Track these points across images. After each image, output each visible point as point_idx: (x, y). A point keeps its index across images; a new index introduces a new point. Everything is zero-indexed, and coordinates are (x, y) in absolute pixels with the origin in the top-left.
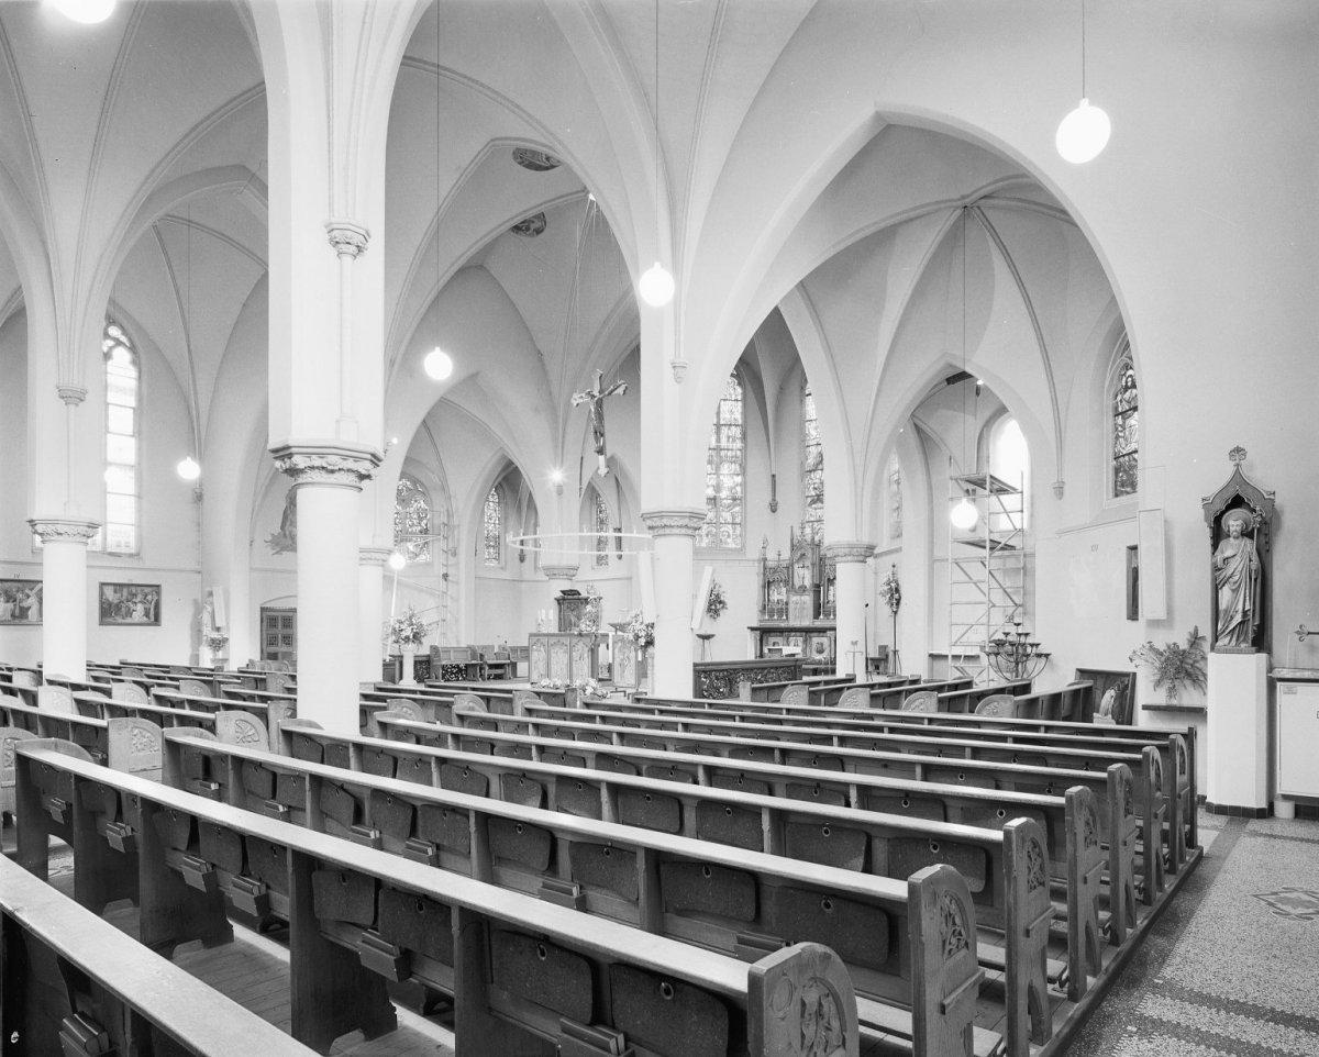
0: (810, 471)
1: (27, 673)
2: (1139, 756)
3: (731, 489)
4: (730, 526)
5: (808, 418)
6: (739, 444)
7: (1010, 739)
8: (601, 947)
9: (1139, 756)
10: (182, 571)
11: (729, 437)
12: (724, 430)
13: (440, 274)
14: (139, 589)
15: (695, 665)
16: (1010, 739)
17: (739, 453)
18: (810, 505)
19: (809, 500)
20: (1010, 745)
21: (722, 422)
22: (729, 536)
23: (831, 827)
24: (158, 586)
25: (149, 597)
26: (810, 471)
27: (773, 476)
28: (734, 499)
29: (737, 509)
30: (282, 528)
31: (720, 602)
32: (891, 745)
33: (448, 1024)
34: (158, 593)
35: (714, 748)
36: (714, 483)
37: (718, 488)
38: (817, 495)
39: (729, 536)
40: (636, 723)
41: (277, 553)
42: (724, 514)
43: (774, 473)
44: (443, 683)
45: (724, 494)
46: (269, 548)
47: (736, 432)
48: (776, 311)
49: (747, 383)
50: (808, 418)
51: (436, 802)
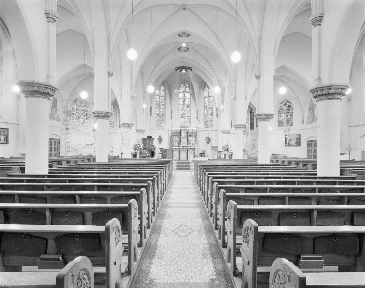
2: (147, 184)
5: (179, 98)
8: (110, 253)
9: (147, 184)
10: (310, 128)
12: (161, 98)
13: (152, 47)
14: (3, 130)
16: (318, 178)
19: (180, 117)
20: (282, 180)
23: (33, 211)
24: (7, 129)
25: (5, 133)
27: (197, 111)
30: (51, 111)
32: (139, 182)
34: (8, 132)
35: (271, 183)
44: (12, 167)
45: (161, 113)
49: (166, 86)
50: (179, 98)
51: (142, 206)
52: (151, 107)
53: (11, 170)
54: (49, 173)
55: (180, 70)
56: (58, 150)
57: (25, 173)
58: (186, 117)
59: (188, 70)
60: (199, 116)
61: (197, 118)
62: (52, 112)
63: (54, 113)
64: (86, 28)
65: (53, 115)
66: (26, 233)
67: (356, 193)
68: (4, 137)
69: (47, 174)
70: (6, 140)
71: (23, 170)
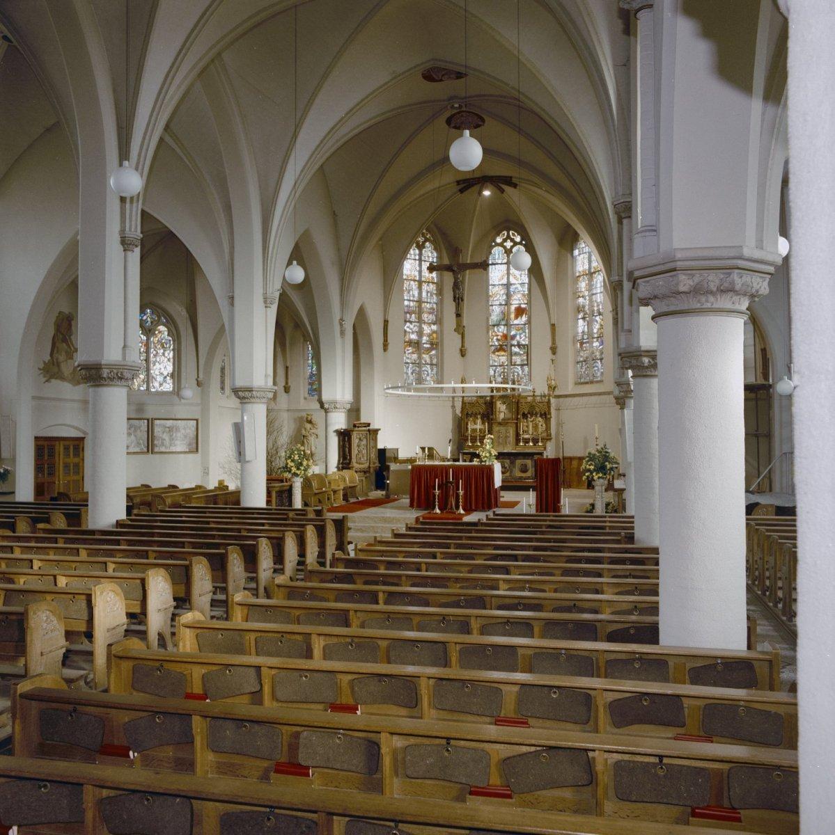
0: (494, 326)
1: (99, 565)
3: (429, 335)
4: (428, 366)
6: (435, 299)
7: (473, 531)
11: (428, 292)
12: (425, 287)
15: (37, 438)
16: (473, 531)
17: (435, 306)
18: (494, 352)
19: (493, 348)
21: (423, 279)
22: (428, 375)
26: (494, 326)
28: (432, 344)
29: (433, 352)
30: (51, 355)
31: (310, 422)
33: (18, 833)
36: (417, 330)
37: (420, 333)
38: (500, 345)
39: (428, 375)
40: (394, 554)
41: (47, 381)
42: (424, 356)
43: (553, 322)
45: (425, 339)
46: (42, 376)
47: (432, 287)
48: (143, 212)
52: (386, 322)
58: (516, 349)
59: (504, 187)
62: (55, 355)
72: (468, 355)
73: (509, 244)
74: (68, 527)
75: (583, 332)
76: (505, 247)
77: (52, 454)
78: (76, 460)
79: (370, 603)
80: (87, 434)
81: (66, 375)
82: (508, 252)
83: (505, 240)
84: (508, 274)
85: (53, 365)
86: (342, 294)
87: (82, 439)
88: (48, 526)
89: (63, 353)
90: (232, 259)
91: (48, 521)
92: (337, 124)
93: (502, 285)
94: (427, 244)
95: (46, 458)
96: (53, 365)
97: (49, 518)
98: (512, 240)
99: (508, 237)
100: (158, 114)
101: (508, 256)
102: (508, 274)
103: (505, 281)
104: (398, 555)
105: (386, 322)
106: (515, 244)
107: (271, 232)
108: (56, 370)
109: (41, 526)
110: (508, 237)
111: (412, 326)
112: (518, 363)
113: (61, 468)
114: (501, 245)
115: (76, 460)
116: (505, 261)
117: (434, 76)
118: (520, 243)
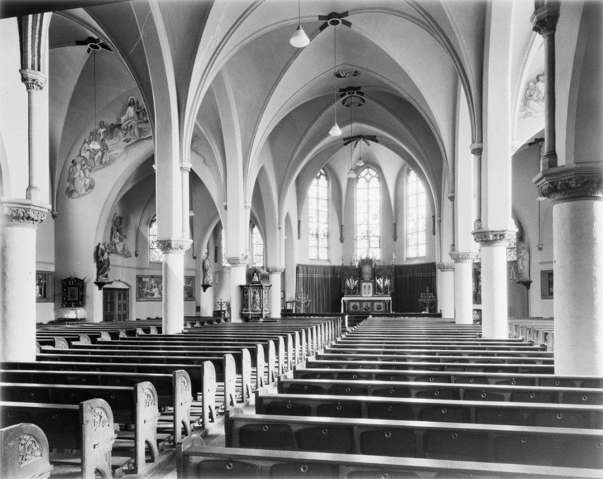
25: (42, 281)
52: (299, 221)
53: (78, 340)
54: (38, 358)
55: (354, 143)
56: (125, 309)
57: (162, 333)
59: (370, 142)
60: (344, 236)
61: (342, 240)
62: (113, 239)
63: (117, 241)
64: (515, 96)
65: (115, 246)
66: (269, 401)
67: (550, 426)
68: (40, 288)
69: (33, 360)
70: (43, 293)
71: (159, 329)
72: (345, 241)
73: (368, 177)
74: (69, 348)
75: (413, 228)
76: (366, 179)
77: (112, 298)
78: (125, 302)
79: (580, 387)
80: (131, 287)
81: (119, 251)
82: (368, 181)
83: (366, 174)
84: (368, 194)
85: (112, 245)
86: (279, 205)
87: (127, 290)
88: (50, 348)
89: (117, 238)
90: (226, 182)
91: (53, 344)
92: (288, 101)
93: (365, 201)
94: (322, 176)
95: (109, 300)
96: (112, 245)
97: (54, 342)
98: (370, 175)
99: (368, 172)
100: (201, 90)
101: (368, 184)
102: (368, 194)
103: (366, 199)
104: (341, 366)
105: (299, 221)
106: (372, 177)
107: (441, 139)
108: (113, 248)
109: (74, 343)
110: (368, 172)
111: (313, 225)
112: (120, 269)
113: (117, 307)
114: (364, 177)
115: (125, 302)
116: (366, 187)
117: (341, 74)
118: (375, 176)
